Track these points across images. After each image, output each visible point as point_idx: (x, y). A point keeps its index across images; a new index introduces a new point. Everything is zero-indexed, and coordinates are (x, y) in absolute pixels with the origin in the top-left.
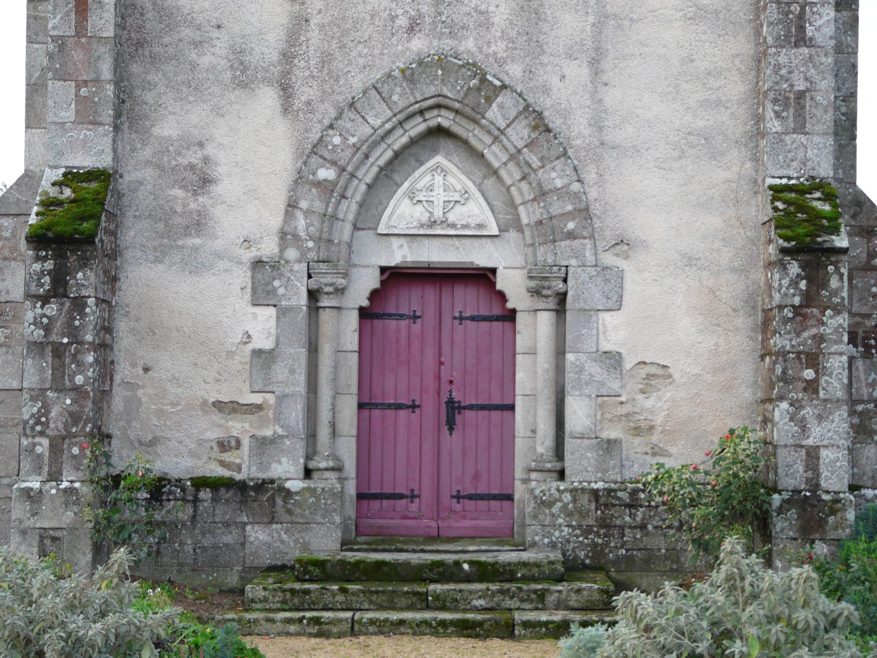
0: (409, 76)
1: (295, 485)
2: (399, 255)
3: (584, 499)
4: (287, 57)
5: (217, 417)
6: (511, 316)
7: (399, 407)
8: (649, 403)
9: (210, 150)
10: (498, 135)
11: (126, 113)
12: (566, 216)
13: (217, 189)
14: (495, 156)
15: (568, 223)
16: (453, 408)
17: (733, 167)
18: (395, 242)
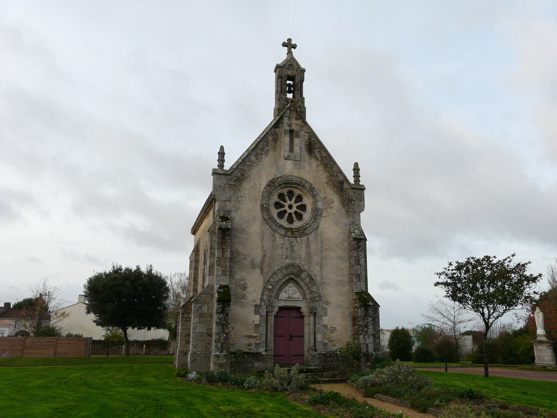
0: (287, 267)
1: (264, 353)
2: (282, 304)
3: (321, 356)
4: (262, 263)
5: (247, 339)
6: (303, 317)
7: (281, 336)
8: (333, 335)
9: (246, 281)
10: (303, 280)
11: (231, 275)
12: (317, 297)
13: (248, 290)
14: (302, 284)
15: (316, 299)
16: (291, 336)
17: (346, 288)
18: (282, 301)
